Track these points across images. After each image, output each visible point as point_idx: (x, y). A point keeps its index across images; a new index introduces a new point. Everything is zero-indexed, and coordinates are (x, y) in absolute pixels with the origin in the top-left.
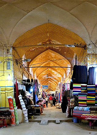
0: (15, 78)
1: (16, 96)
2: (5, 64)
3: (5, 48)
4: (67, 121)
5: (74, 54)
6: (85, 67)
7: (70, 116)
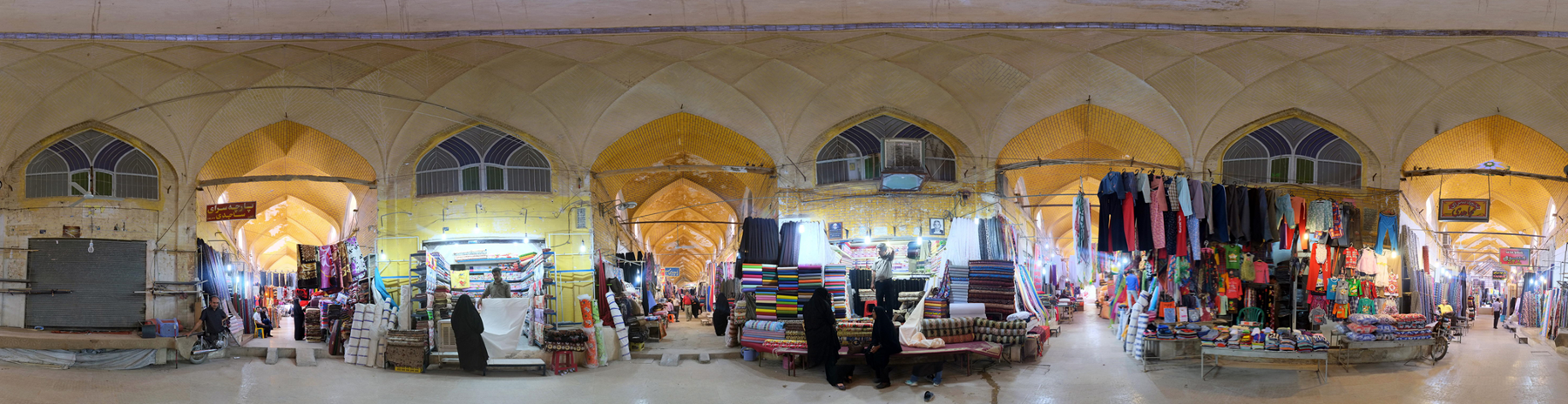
0: (598, 250)
2: (573, 214)
3: (572, 174)
4: (726, 356)
5: (743, 190)
7: (735, 344)
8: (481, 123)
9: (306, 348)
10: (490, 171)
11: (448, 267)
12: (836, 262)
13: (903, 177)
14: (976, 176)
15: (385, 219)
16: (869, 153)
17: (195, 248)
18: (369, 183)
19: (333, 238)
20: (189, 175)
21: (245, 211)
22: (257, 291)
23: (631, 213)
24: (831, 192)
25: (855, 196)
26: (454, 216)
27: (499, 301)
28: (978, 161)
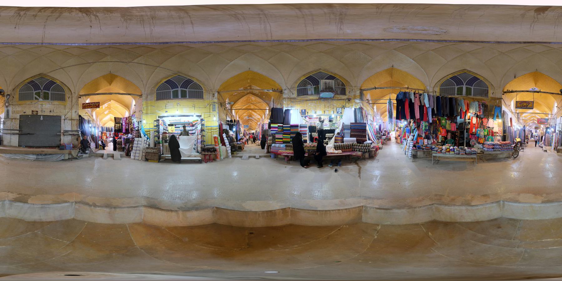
0: (220, 119)
2: (211, 106)
3: (211, 92)
4: (265, 157)
5: (271, 98)
6: (282, 109)
7: (268, 152)
9: (117, 154)
11: (167, 125)
12: (304, 123)
13: (327, 93)
16: (315, 85)
18: (139, 96)
19: (127, 115)
20: (76, 93)
23: (232, 106)
24: (302, 99)
25: (310, 100)
27: (185, 137)
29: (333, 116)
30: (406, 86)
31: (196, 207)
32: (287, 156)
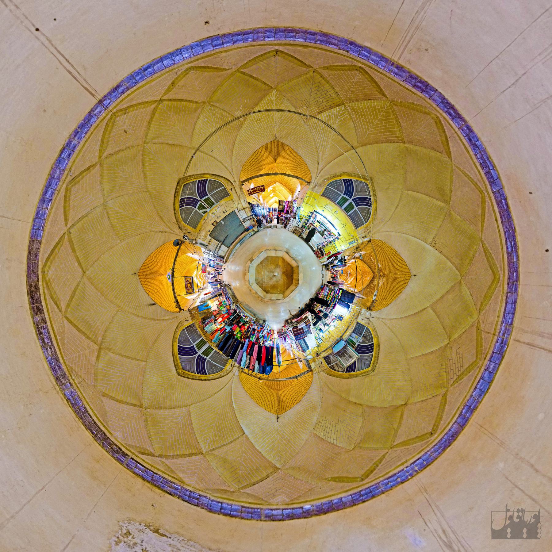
0: (344, 251)
1: (333, 255)
2: (353, 240)
3: (367, 233)
4: (322, 283)
5: (366, 296)
6: (351, 302)
7: (325, 285)
8: (368, 182)
9: (279, 225)
10: (351, 204)
11: (316, 220)
12: (333, 313)
13: (340, 348)
14: (318, 363)
15: (308, 197)
16: (357, 347)
17: (248, 206)
18: (308, 182)
19: (290, 199)
20: (236, 180)
21: (261, 189)
22: (268, 213)
23: (358, 258)
24: (352, 325)
25: (346, 330)
26: (328, 209)
27: (320, 236)
28: (320, 370)
29: (321, 334)
30: (261, 381)
31: (296, 261)
32: (319, 294)
